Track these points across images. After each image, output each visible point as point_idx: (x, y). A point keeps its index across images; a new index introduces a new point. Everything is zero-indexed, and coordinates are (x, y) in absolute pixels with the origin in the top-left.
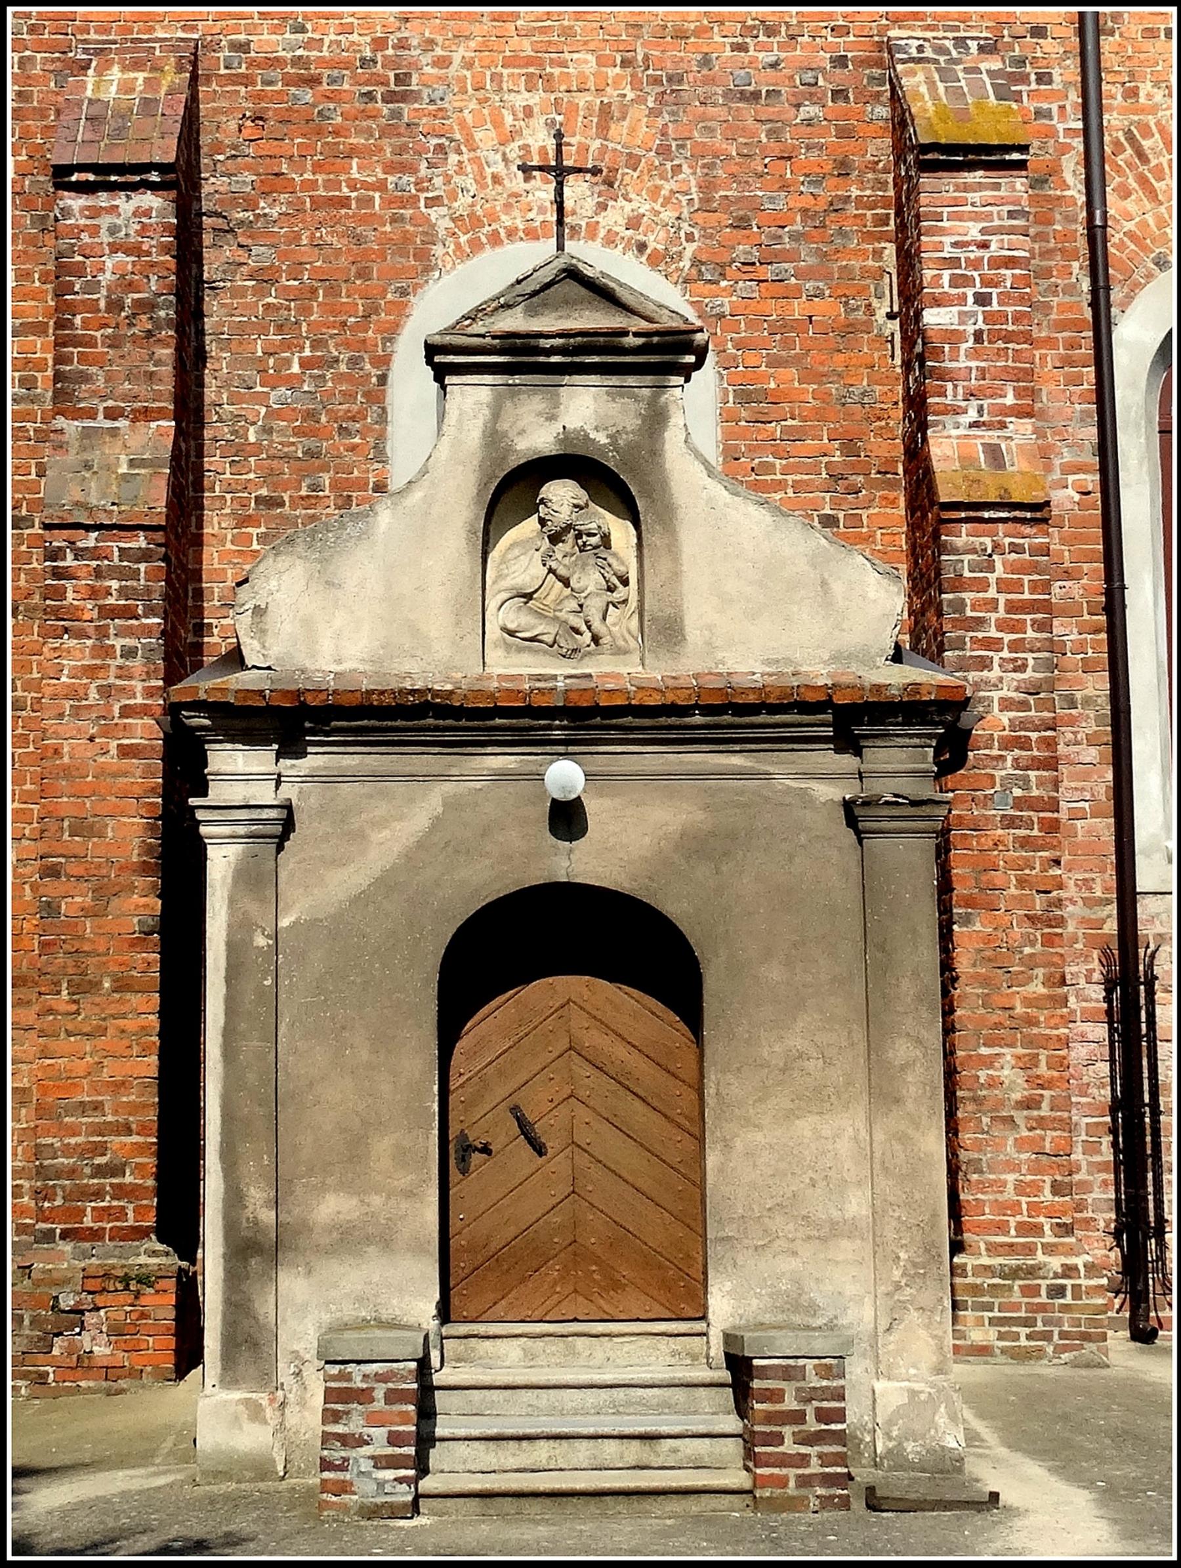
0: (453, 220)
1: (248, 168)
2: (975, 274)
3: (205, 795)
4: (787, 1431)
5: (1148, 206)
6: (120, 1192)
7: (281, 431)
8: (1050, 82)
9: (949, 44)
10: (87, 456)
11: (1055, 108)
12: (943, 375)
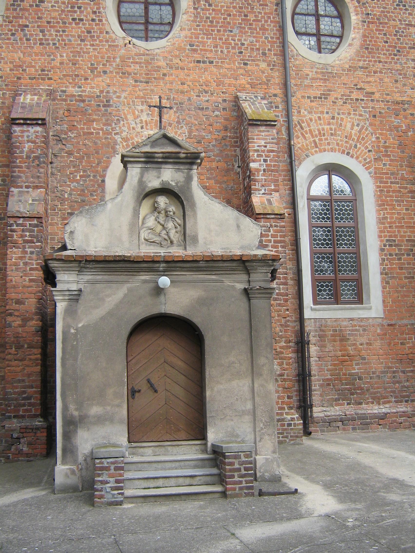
0: (122, 139)
1: (65, 124)
2: (263, 154)
3: (56, 287)
4: (236, 474)
5: (304, 141)
6: (30, 404)
7: (74, 195)
8: (278, 108)
9: (253, 97)
10: (21, 198)
11: (280, 115)
12: (255, 181)
